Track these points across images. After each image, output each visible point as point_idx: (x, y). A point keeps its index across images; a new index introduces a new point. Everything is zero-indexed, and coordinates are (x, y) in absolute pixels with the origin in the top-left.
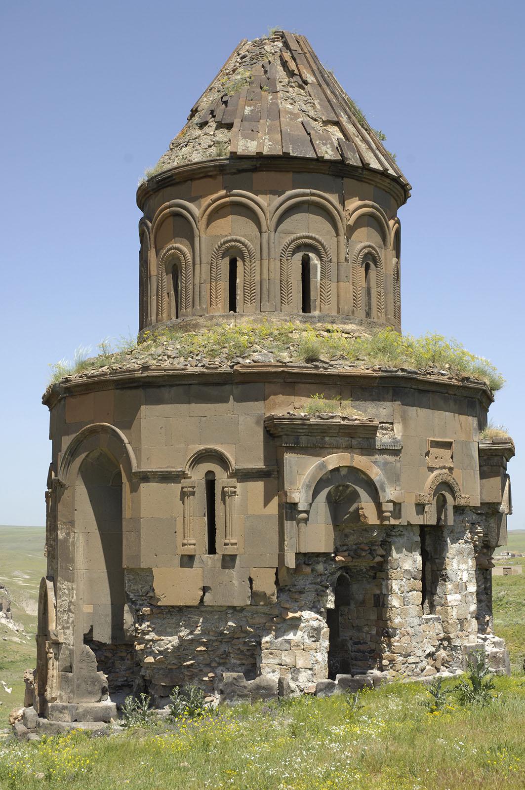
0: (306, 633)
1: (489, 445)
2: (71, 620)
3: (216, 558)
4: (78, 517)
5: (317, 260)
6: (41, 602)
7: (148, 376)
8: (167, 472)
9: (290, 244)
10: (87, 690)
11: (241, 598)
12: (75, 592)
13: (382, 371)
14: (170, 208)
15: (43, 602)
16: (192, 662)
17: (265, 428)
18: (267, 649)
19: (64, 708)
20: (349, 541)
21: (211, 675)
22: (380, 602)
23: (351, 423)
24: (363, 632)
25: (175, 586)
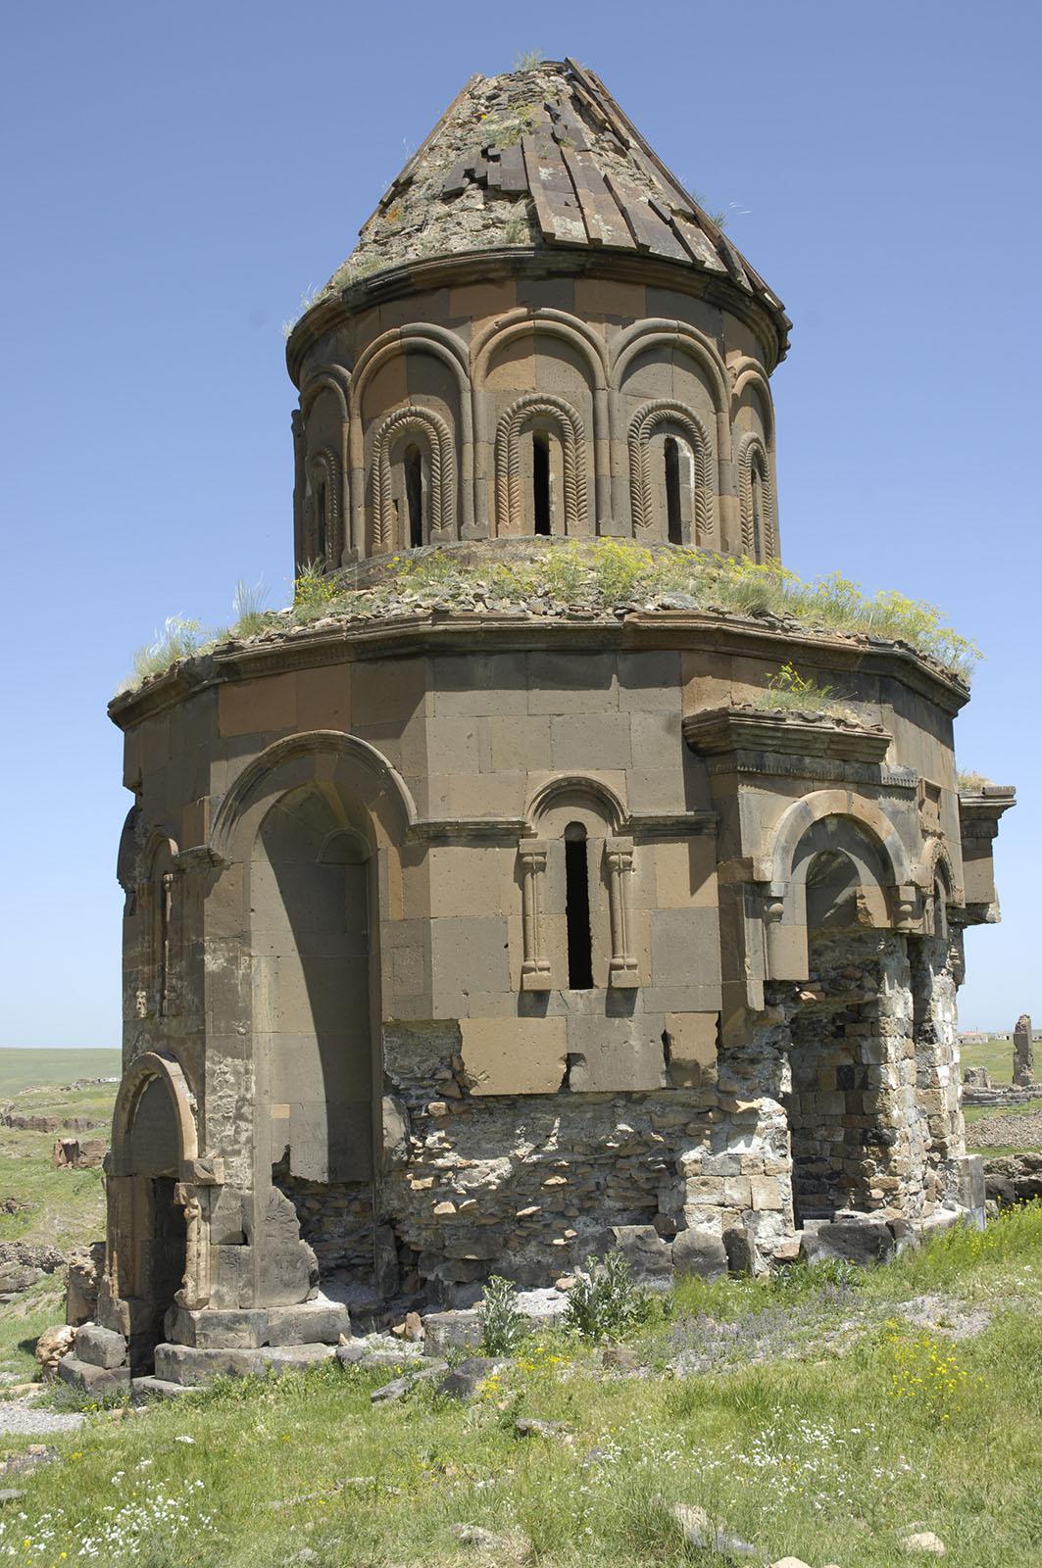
0: (768, 1141)
1: (980, 800)
2: (243, 1138)
3: (592, 996)
4: (257, 925)
6: (123, 1108)
7: (446, 631)
8: (487, 823)
9: (647, 415)
11: (645, 1074)
12: (254, 1078)
13: (871, 643)
14: (401, 338)
15: (128, 1106)
16: (534, 1208)
17: (685, 738)
18: (696, 1175)
19: (237, 1319)
21: (569, 1233)
22: (853, 1079)
23: (849, 731)
24: (813, 1139)
25: (508, 1055)
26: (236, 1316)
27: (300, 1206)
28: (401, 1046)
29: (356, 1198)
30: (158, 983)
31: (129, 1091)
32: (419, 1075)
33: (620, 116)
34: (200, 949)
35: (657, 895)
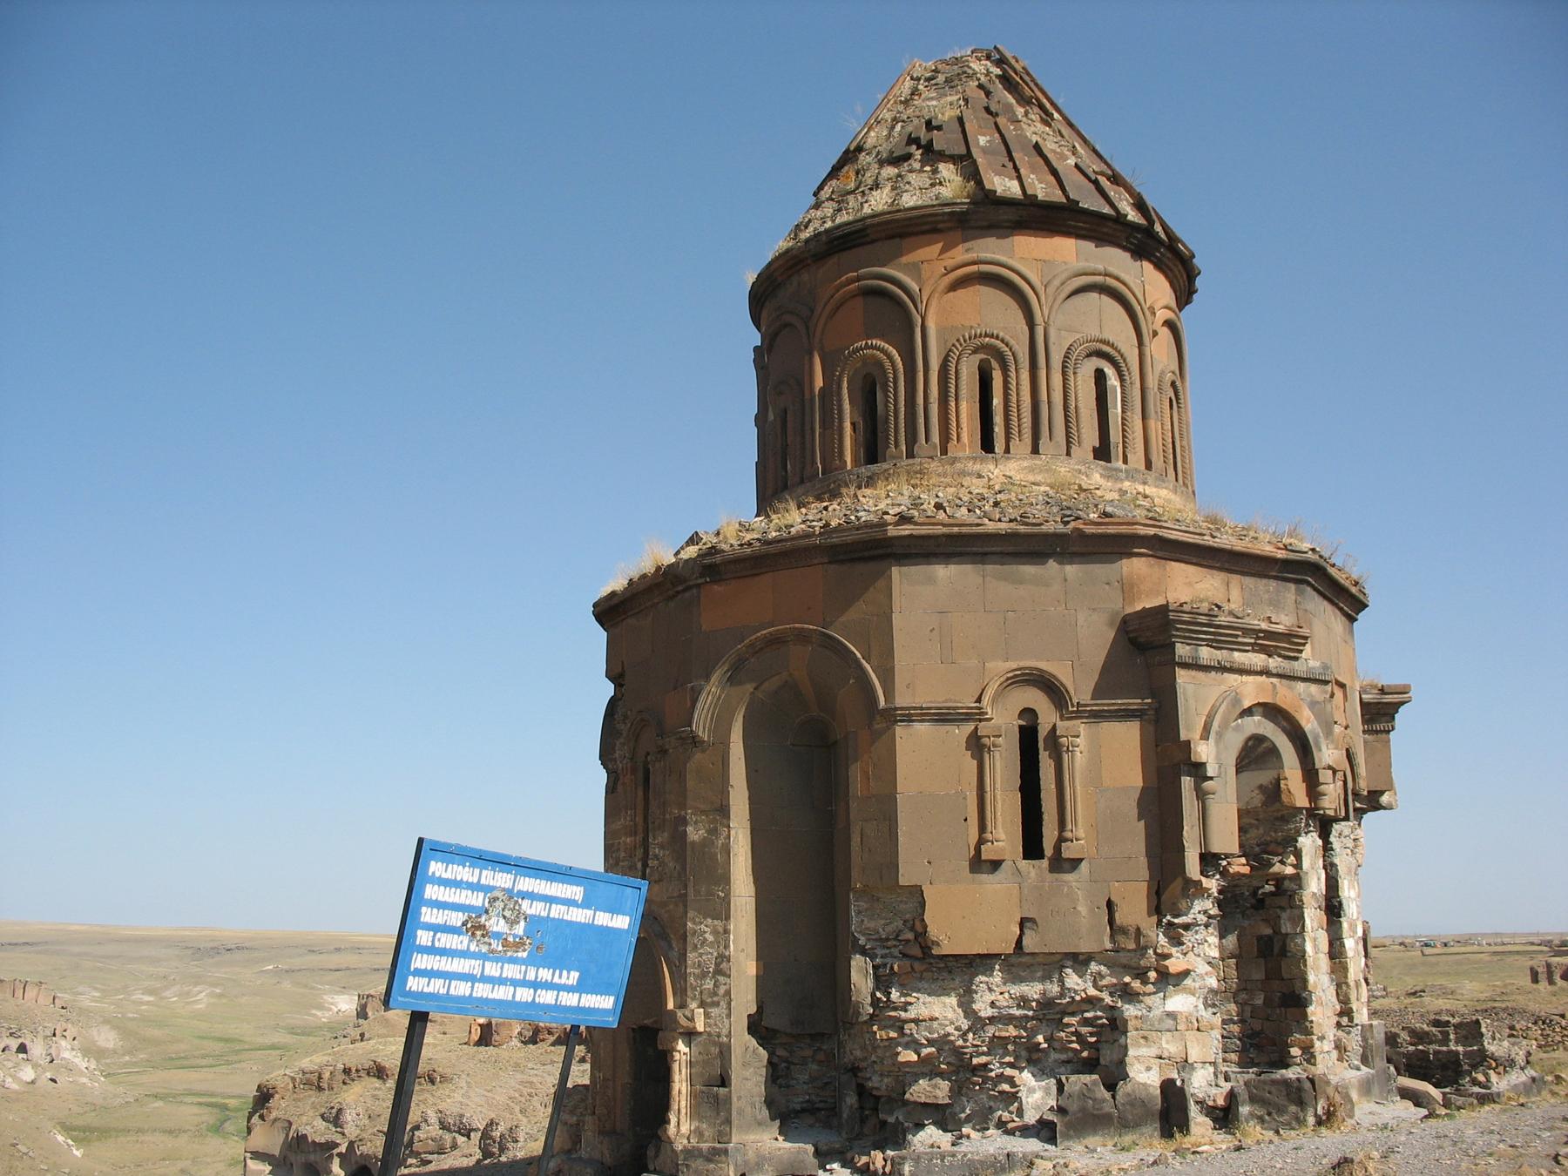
2: (722, 990)
25: (967, 914)
27: (771, 1054)
29: (820, 1049)
30: (639, 853)
33: (1044, 93)
34: (685, 822)
35: (1103, 762)
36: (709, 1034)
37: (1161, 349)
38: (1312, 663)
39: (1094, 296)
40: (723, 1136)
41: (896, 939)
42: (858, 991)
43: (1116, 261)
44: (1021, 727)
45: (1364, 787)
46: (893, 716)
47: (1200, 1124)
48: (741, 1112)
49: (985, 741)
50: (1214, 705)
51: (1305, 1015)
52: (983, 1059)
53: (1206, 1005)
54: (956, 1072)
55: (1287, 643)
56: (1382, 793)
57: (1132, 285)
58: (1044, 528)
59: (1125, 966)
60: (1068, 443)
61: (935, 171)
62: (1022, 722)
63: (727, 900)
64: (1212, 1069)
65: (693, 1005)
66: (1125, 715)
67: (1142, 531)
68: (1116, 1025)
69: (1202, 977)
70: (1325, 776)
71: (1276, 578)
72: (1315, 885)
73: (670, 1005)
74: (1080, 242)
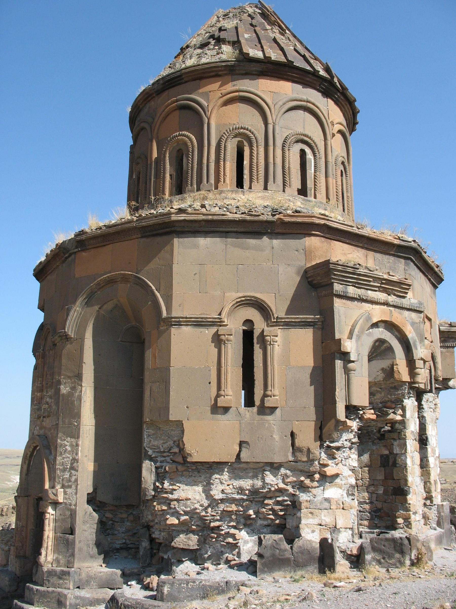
2: (73, 479)
5: (311, 156)
6: (25, 463)
7: (185, 220)
10: (89, 554)
15: (27, 462)
18: (307, 508)
20: (375, 399)
25: (206, 438)
26: (63, 571)
28: (153, 434)
31: (27, 454)
32: (162, 450)
33: (279, 18)
34: (59, 383)
35: (291, 352)
36: (66, 504)
37: (337, 143)
38: (413, 301)
39: (301, 112)
40: (70, 564)
41: (168, 452)
42: (146, 482)
43: (313, 96)
44: (244, 331)
45: (441, 375)
46: (171, 322)
47: (342, 565)
48: (80, 550)
49: (223, 337)
50: (356, 321)
51: (406, 500)
52: (217, 524)
53: (348, 494)
54: (202, 530)
55: (399, 288)
56: (449, 379)
57: (321, 108)
58: (261, 218)
59: (301, 471)
60: (284, 185)
61: (220, 48)
62: (245, 328)
63: (78, 428)
64: (350, 532)
65: (58, 487)
66: (304, 324)
67: (317, 221)
68: (295, 505)
69: (346, 478)
70: (419, 364)
71: (394, 255)
72: (413, 427)
73: (47, 486)
74: (293, 84)
